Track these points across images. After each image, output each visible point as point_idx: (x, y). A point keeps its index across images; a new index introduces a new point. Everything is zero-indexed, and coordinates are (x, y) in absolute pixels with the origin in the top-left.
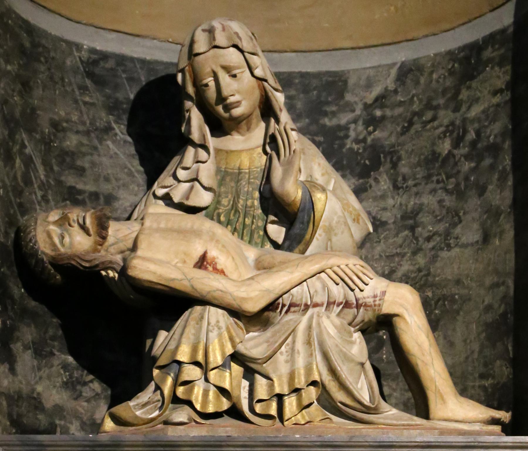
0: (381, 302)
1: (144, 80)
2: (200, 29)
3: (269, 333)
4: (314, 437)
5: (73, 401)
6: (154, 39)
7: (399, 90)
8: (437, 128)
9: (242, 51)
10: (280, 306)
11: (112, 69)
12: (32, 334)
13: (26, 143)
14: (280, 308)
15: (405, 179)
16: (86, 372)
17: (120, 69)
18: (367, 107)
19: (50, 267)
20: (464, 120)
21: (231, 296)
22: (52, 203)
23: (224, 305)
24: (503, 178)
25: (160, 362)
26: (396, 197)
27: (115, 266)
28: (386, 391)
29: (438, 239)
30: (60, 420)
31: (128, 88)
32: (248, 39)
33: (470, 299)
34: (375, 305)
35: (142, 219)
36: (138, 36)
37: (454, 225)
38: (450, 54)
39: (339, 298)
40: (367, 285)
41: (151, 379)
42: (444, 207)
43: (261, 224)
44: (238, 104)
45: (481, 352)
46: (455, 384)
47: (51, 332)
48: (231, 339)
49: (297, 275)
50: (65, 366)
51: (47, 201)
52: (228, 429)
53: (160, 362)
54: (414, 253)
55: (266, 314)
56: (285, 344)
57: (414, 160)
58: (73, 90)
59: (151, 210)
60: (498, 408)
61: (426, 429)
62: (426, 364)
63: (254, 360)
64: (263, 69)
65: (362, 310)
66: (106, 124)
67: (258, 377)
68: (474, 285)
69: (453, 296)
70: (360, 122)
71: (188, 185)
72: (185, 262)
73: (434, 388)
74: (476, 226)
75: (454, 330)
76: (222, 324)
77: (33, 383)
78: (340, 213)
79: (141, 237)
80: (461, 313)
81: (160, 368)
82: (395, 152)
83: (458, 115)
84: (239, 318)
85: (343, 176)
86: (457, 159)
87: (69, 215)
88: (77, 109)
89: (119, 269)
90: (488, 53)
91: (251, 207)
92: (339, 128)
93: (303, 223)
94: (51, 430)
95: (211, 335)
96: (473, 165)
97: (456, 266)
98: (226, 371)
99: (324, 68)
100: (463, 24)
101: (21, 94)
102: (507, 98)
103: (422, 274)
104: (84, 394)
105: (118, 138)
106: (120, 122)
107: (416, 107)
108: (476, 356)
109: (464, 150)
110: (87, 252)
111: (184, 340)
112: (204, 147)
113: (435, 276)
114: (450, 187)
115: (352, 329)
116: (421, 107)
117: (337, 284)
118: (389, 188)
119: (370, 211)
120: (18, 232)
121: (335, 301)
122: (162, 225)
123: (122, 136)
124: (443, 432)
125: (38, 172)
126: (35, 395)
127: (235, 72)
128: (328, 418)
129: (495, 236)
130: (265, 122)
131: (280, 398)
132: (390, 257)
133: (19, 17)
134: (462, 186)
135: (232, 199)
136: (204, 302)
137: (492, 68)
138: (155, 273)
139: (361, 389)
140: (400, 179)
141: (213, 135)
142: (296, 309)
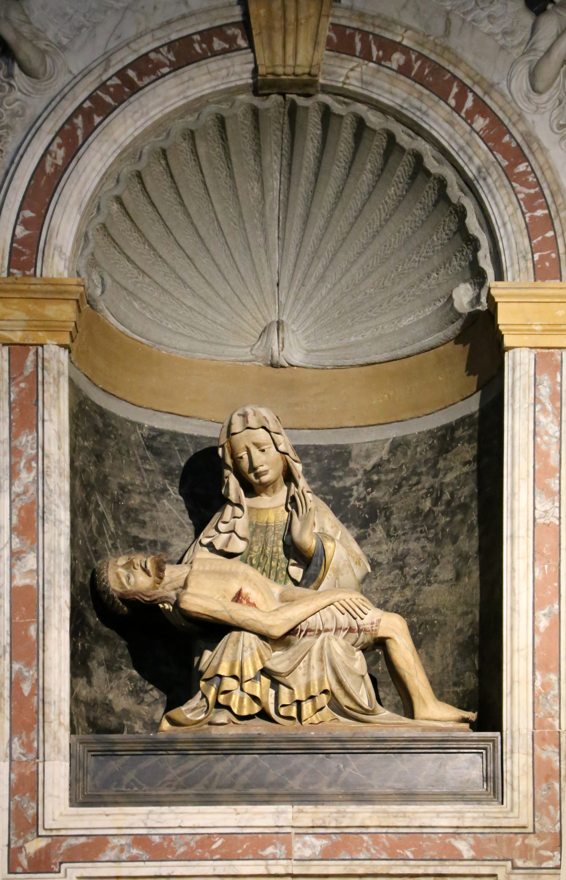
0: (377, 628)
1: (192, 452)
2: (236, 414)
3: (291, 652)
4: (325, 734)
5: (136, 706)
6: (200, 419)
8: (421, 490)
11: (167, 443)
12: (104, 654)
13: (100, 503)
16: (147, 682)
17: (173, 443)
18: (366, 472)
19: (119, 601)
20: (442, 484)
22: (120, 550)
23: (256, 631)
24: (471, 529)
25: (206, 676)
26: (389, 543)
27: (170, 600)
28: (382, 695)
29: (421, 577)
30: (127, 720)
32: (274, 422)
33: (445, 624)
35: (191, 563)
36: (187, 417)
37: (434, 566)
41: (199, 689)
42: (426, 551)
43: (284, 566)
44: (266, 472)
45: (454, 665)
46: (434, 690)
47: (120, 651)
48: (261, 657)
49: (312, 607)
50: (131, 678)
51: (116, 548)
52: (259, 728)
53: (206, 676)
54: (403, 588)
55: (288, 637)
57: (403, 515)
58: (136, 460)
59: (198, 555)
60: (467, 709)
61: (411, 726)
63: (279, 674)
64: (286, 446)
65: (362, 634)
67: (281, 687)
68: (448, 612)
69: (433, 621)
70: (361, 485)
71: (227, 535)
72: (224, 597)
74: (450, 567)
75: (434, 647)
76: (254, 646)
77: (105, 692)
78: (346, 558)
79: (191, 578)
80: (439, 635)
81: (206, 680)
82: (388, 508)
83: (437, 480)
84: (267, 642)
85: (348, 527)
87: (134, 560)
88: (139, 475)
89: (173, 603)
90: (459, 433)
92: (345, 489)
93: (316, 566)
94: (119, 730)
95: (245, 654)
96: (448, 519)
97: (435, 598)
99: (333, 442)
100: (441, 410)
101: (95, 465)
102: (474, 468)
103: (409, 604)
104: (146, 700)
107: (404, 473)
108: (450, 668)
109: (441, 508)
110: (148, 590)
111: (224, 658)
112: (240, 506)
113: (419, 606)
114: (430, 536)
115: (355, 649)
116: (409, 473)
117: (343, 614)
120: (93, 573)
122: (207, 568)
123: (175, 496)
124: (424, 729)
125: (109, 525)
126: (107, 702)
127: (263, 448)
129: (465, 576)
130: (287, 485)
131: (299, 703)
132: (384, 590)
133: (93, 403)
136: (239, 629)
137: (463, 444)
138: (201, 606)
139: (362, 696)
140: (392, 529)
141: (246, 496)
142: (312, 633)
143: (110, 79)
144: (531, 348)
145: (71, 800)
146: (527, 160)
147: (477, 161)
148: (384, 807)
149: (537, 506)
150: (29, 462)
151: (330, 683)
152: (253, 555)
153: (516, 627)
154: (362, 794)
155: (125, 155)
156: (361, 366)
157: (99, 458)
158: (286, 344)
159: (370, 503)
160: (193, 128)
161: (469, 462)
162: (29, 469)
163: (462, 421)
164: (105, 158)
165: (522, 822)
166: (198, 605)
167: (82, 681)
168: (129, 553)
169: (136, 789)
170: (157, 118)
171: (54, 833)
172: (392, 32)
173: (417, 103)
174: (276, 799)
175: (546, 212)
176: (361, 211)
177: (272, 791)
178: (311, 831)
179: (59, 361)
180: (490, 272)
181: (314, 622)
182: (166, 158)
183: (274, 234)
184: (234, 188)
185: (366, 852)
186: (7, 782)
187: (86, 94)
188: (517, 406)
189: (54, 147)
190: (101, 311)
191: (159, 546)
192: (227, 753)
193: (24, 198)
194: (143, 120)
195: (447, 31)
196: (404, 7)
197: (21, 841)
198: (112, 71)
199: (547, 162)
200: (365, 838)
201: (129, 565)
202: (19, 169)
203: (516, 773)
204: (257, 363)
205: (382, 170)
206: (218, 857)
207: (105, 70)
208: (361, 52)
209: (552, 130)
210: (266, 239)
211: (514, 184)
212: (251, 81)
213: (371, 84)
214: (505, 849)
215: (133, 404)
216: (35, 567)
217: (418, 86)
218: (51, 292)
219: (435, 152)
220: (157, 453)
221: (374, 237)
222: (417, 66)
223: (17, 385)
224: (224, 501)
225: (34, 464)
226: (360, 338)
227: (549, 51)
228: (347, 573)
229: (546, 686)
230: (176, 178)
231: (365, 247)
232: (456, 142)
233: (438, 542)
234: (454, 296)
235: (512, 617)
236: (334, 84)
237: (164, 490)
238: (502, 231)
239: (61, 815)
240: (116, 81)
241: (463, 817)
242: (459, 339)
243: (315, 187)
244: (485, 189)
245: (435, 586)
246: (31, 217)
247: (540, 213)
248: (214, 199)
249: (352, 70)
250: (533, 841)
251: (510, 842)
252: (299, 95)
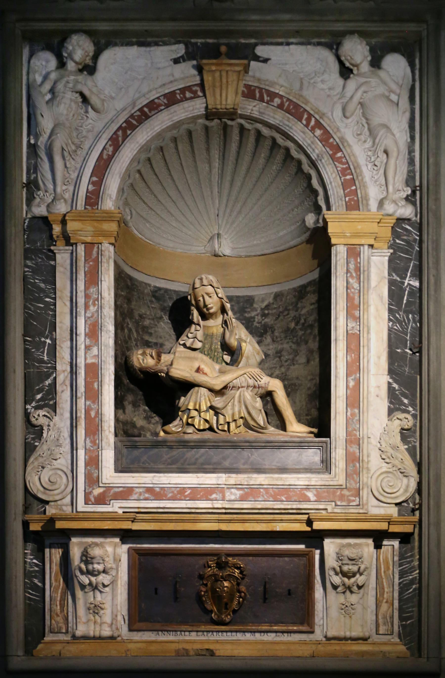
1: (175, 298)
3: (224, 398)
4: (241, 439)
9: (213, 287)
17: (166, 294)
20: (300, 315)
22: (139, 347)
24: (315, 337)
28: (270, 420)
37: (296, 356)
41: (178, 415)
43: (221, 355)
44: (212, 308)
45: (306, 406)
46: (296, 418)
47: (139, 397)
48: (210, 400)
49: (235, 375)
50: (145, 411)
54: (281, 367)
55: (223, 390)
57: (280, 330)
59: (178, 349)
63: (218, 408)
67: (220, 415)
71: (192, 340)
74: (304, 356)
76: (206, 394)
78: (252, 351)
79: (175, 360)
81: (182, 411)
85: (253, 337)
90: (309, 289)
94: (139, 436)
96: (303, 332)
99: (245, 294)
107: (281, 309)
108: (304, 407)
109: (299, 327)
110: (153, 366)
111: (191, 401)
112: (199, 325)
114: (294, 341)
122: (183, 356)
124: (291, 437)
131: (228, 423)
132: (271, 368)
133: (126, 274)
136: (199, 386)
141: (202, 320)
143: (135, 112)
144: (345, 245)
145: (115, 469)
146: (342, 151)
147: (317, 151)
148: (271, 475)
149: (349, 324)
150: (94, 302)
151: (244, 413)
152: (206, 349)
153: (338, 385)
154: (260, 469)
155: (142, 150)
156: (259, 256)
157: (129, 301)
158: (222, 244)
160: (176, 136)
161: (313, 304)
162: (94, 305)
163: (310, 283)
164: (132, 151)
165: (340, 483)
167: (120, 411)
168: (144, 348)
169: (147, 464)
170: (158, 131)
171: (107, 485)
172: (274, 88)
173: (287, 123)
174: (217, 470)
175: (352, 177)
176: (259, 178)
177: (215, 467)
178: (234, 487)
179: (109, 251)
180: (324, 207)
181: (237, 382)
182: (162, 152)
183: (216, 190)
184: (196, 167)
185: (261, 497)
186: (84, 460)
187: (124, 120)
188: (338, 274)
189: (108, 146)
190: (130, 227)
191: (159, 346)
192: (192, 447)
193: (93, 171)
194: (151, 132)
195: (301, 88)
196: (280, 76)
197: (91, 489)
198: (136, 108)
199: (352, 152)
200: (262, 490)
201: (144, 354)
202: (90, 157)
203: (337, 459)
205: (270, 157)
206: (188, 499)
207: (133, 108)
208: (259, 98)
209: (354, 136)
210: (212, 192)
211: (336, 163)
212: (204, 112)
213: (264, 113)
214: (331, 496)
216: (97, 354)
217: (287, 114)
218: (106, 217)
219: (296, 147)
220: (158, 299)
221: (266, 191)
222: (286, 104)
223: (89, 263)
224: (191, 322)
225: (97, 303)
226: (259, 242)
227: (352, 97)
229: (353, 415)
230: (168, 161)
231: (261, 196)
232: (306, 142)
233: (298, 344)
234: (306, 219)
235: (336, 380)
236: (246, 113)
237: (161, 318)
238: (330, 186)
239: (110, 476)
240: (138, 113)
241: (310, 480)
242: (308, 241)
243: (236, 167)
244: (321, 165)
245: (296, 366)
246: (96, 181)
247: (348, 177)
248: (186, 172)
249: (254, 106)
250: (346, 492)
251: (334, 493)
252: (228, 119)
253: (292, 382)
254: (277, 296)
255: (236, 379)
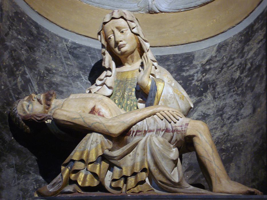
0: (185, 129)
7: (217, 55)
9: (126, 20)
10: (132, 132)
13: (27, 73)
14: (132, 133)
15: (219, 94)
17: (88, 53)
18: (203, 65)
19: (22, 122)
21: (104, 125)
31: (91, 61)
33: (247, 143)
34: (182, 131)
37: (240, 109)
38: (241, 34)
39: (163, 127)
40: (178, 120)
42: (236, 102)
47: (30, 162)
54: (222, 127)
56: (132, 151)
62: (210, 161)
65: (175, 133)
66: (78, 75)
69: (239, 143)
70: (200, 72)
73: (215, 175)
74: (250, 106)
75: (240, 160)
83: (243, 59)
86: (242, 79)
91: (130, 96)
92: (190, 76)
96: (249, 79)
98: (98, 164)
99: (184, 52)
103: (225, 136)
105: (83, 81)
106: (85, 74)
107: (224, 61)
108: (250, 171)
109: (245, 74)
113: (231, 136)
115: (172, 146)
117: (162, 120)
118: (211, 99)
119: (202, 111)
121: (161, 129)
123: (86, 81)
125: (33, 87)
127: (122, 30)
128: (152, 190)
131: (126, 178)
134: (244, 90)
135: (122, 93)
138: (66, 116)
140: (216, 94)
142: (140, 133)
156: (201, 6)
159: (204, 82)
166: (64, 115)
204: (141, 12)
215: (62, 28)
220: (76, 57)
228: (173, 103)
233: (243, 94)
253: (236, 142)
254: (221, 47)
255: (142, 120)
